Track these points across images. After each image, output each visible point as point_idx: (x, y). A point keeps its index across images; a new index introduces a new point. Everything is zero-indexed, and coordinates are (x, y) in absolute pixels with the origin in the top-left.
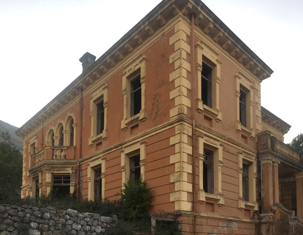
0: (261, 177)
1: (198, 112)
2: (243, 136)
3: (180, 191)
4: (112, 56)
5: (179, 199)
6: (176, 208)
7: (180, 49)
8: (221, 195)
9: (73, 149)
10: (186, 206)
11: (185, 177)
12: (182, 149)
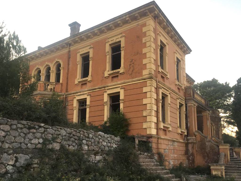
0: (188, 114)
2: (179, 89)
3: (151, 122)
4: (99, 29)
5: (150, 127)
6: (148, 133)
7: (150, 35)
8: (170, 125)
9: (61, 85)
10: (154, 132)
11: (154, 113)
12: (152, 96)
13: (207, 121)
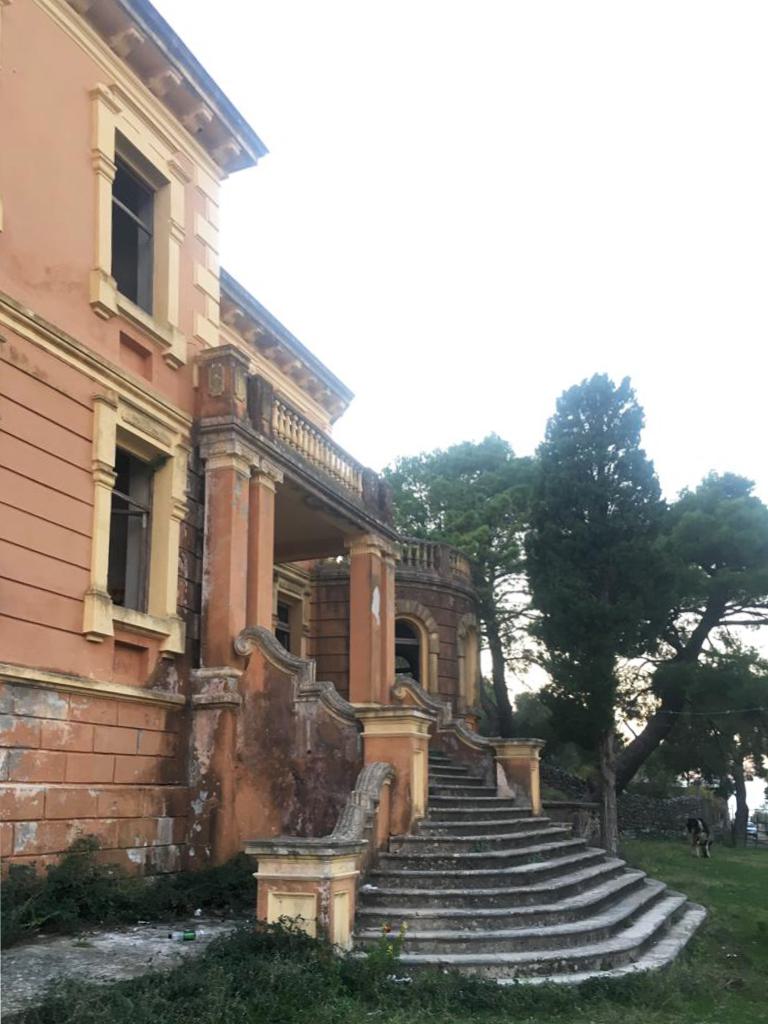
0: (206, 523)
1: (166, 367)
13: (372, 591)
